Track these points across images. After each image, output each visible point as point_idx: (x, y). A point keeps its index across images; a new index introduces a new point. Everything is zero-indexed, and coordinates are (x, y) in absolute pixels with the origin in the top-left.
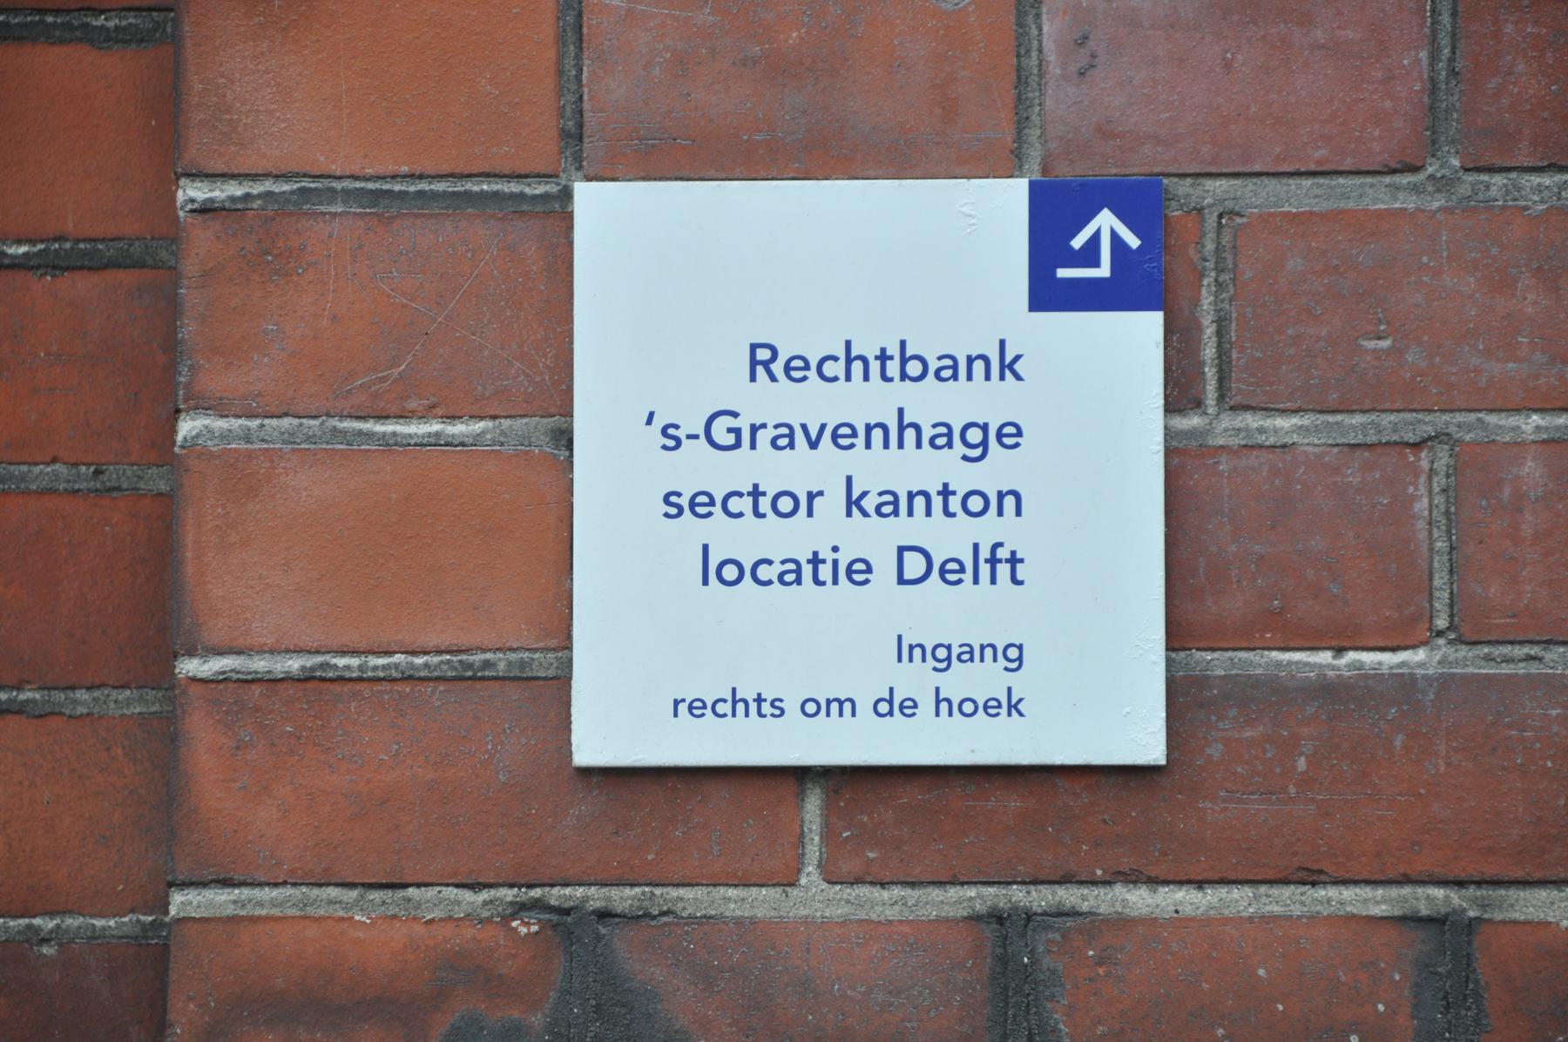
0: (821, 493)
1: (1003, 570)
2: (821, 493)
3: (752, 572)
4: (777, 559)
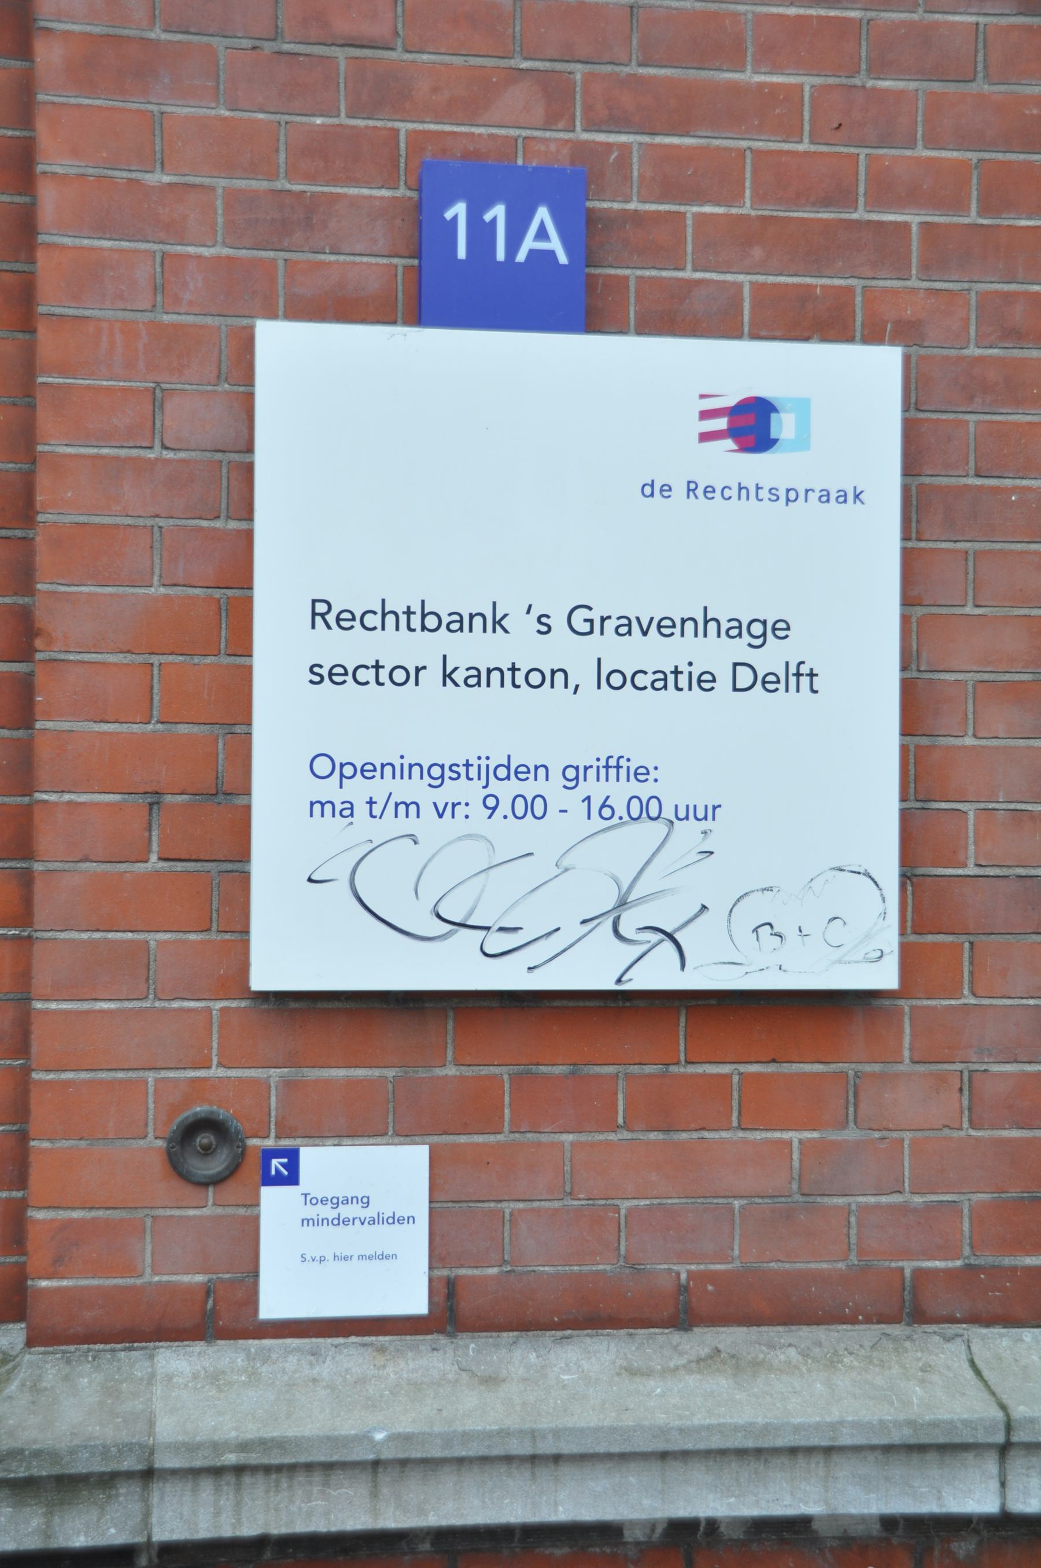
0: (424, 668)
1: (805, 681)
2: (424, 668)
3: (631, 680)
4: (650, 671)
